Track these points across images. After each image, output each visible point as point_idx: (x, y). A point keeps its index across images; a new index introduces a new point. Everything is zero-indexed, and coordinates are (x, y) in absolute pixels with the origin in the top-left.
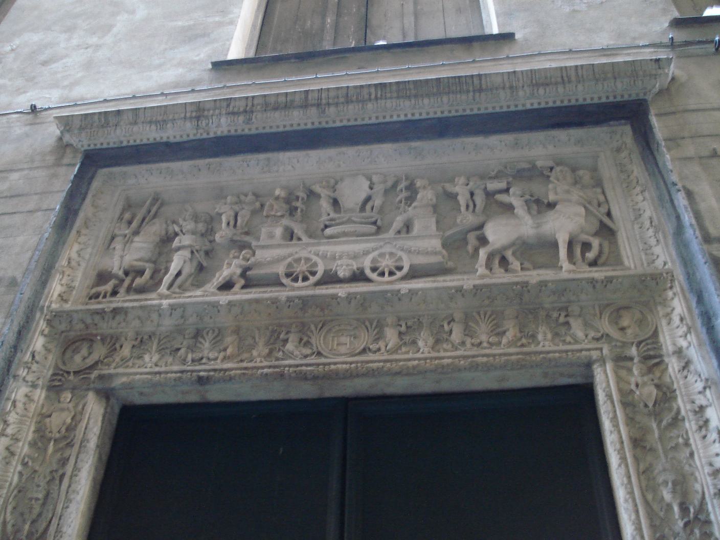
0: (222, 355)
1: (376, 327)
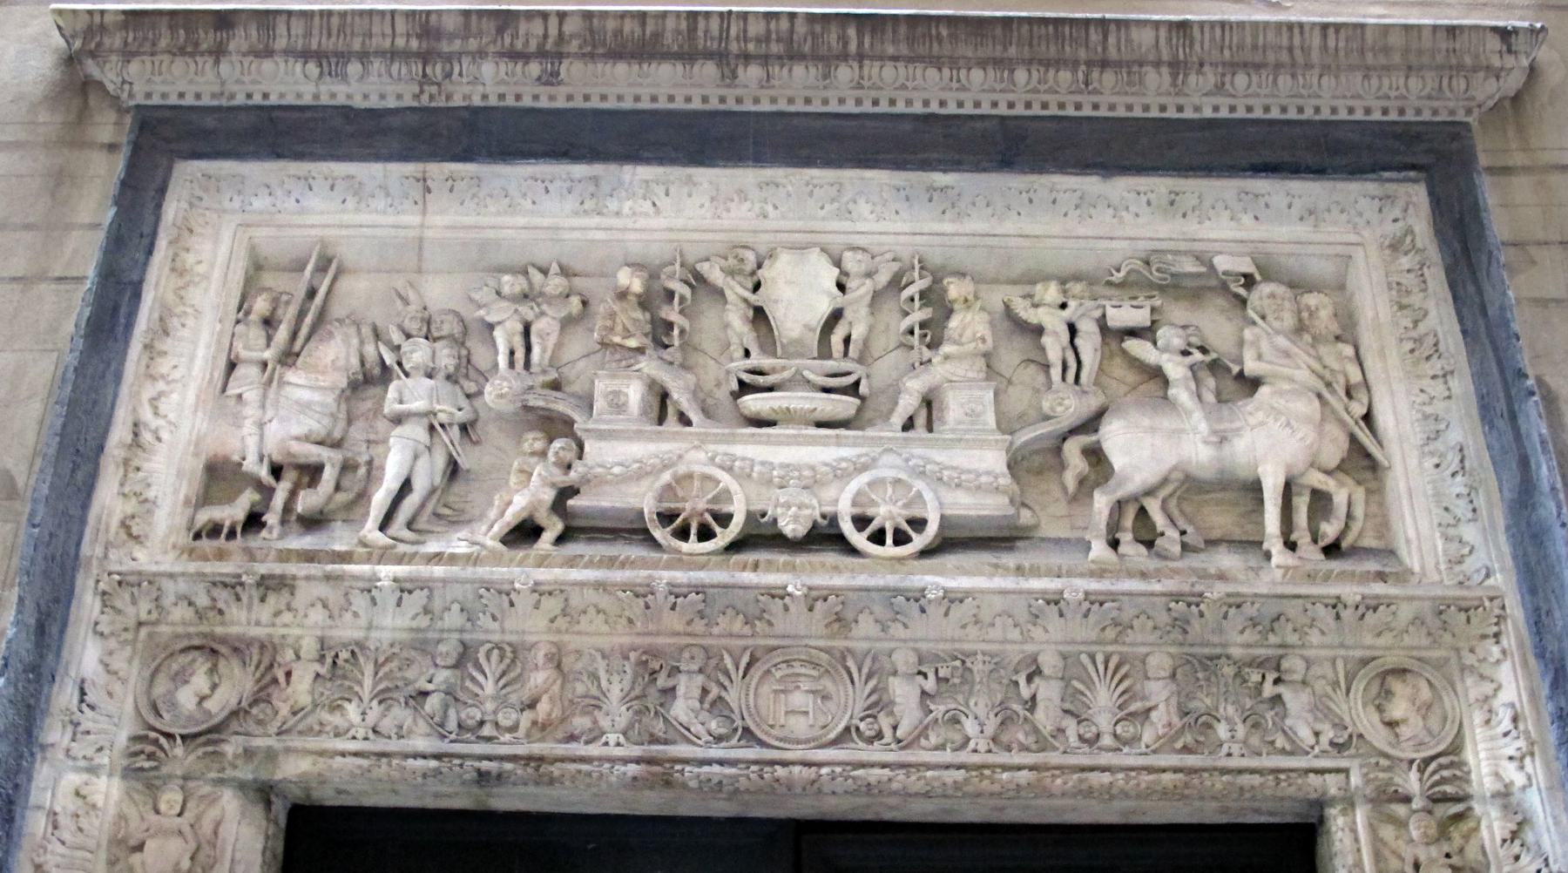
0: (526, 719)
1: (869, 677)
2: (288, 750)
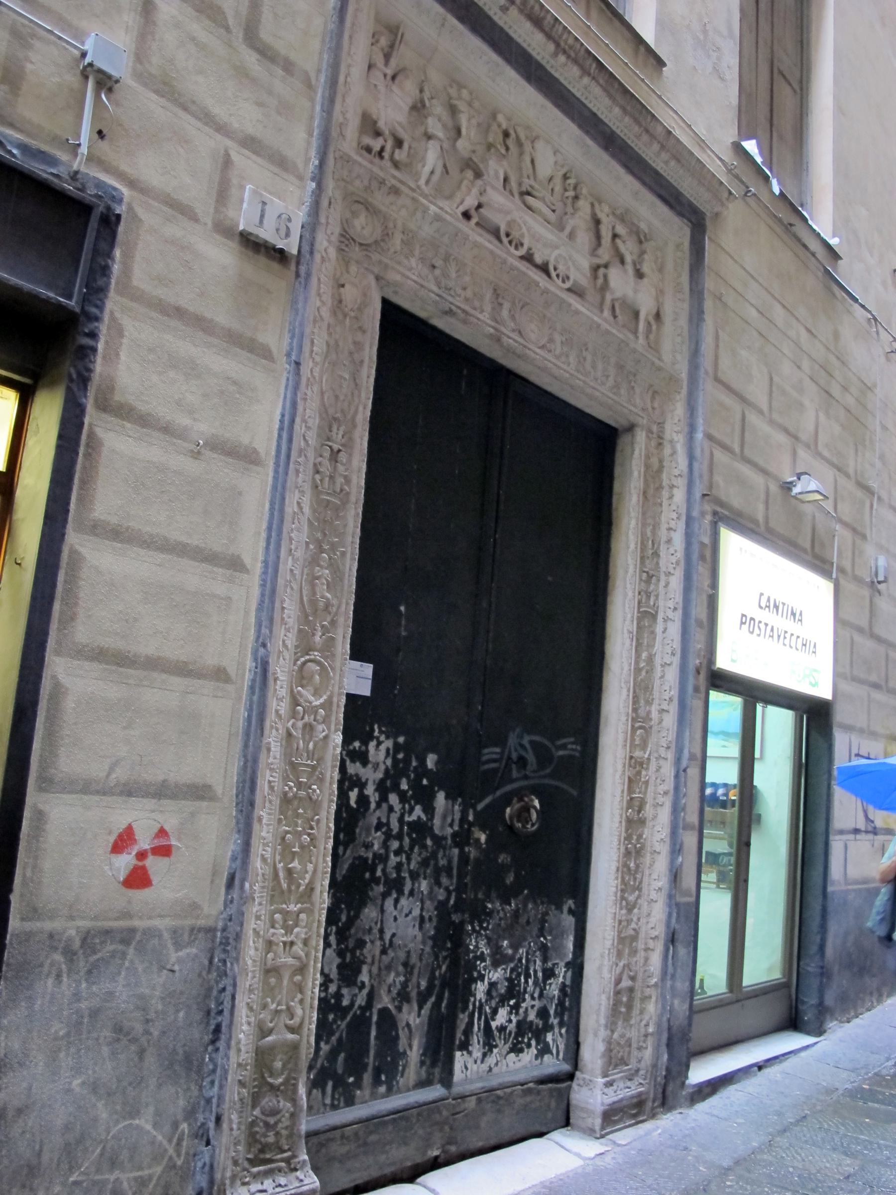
2: (393, 268)
